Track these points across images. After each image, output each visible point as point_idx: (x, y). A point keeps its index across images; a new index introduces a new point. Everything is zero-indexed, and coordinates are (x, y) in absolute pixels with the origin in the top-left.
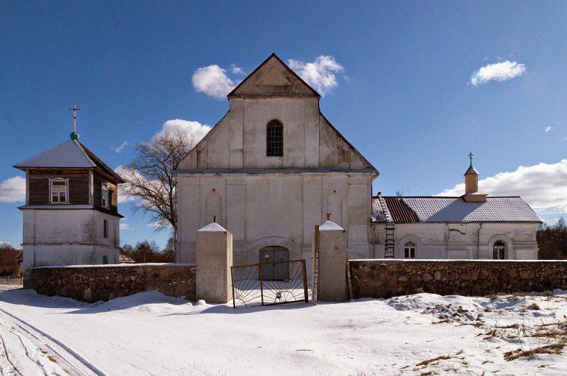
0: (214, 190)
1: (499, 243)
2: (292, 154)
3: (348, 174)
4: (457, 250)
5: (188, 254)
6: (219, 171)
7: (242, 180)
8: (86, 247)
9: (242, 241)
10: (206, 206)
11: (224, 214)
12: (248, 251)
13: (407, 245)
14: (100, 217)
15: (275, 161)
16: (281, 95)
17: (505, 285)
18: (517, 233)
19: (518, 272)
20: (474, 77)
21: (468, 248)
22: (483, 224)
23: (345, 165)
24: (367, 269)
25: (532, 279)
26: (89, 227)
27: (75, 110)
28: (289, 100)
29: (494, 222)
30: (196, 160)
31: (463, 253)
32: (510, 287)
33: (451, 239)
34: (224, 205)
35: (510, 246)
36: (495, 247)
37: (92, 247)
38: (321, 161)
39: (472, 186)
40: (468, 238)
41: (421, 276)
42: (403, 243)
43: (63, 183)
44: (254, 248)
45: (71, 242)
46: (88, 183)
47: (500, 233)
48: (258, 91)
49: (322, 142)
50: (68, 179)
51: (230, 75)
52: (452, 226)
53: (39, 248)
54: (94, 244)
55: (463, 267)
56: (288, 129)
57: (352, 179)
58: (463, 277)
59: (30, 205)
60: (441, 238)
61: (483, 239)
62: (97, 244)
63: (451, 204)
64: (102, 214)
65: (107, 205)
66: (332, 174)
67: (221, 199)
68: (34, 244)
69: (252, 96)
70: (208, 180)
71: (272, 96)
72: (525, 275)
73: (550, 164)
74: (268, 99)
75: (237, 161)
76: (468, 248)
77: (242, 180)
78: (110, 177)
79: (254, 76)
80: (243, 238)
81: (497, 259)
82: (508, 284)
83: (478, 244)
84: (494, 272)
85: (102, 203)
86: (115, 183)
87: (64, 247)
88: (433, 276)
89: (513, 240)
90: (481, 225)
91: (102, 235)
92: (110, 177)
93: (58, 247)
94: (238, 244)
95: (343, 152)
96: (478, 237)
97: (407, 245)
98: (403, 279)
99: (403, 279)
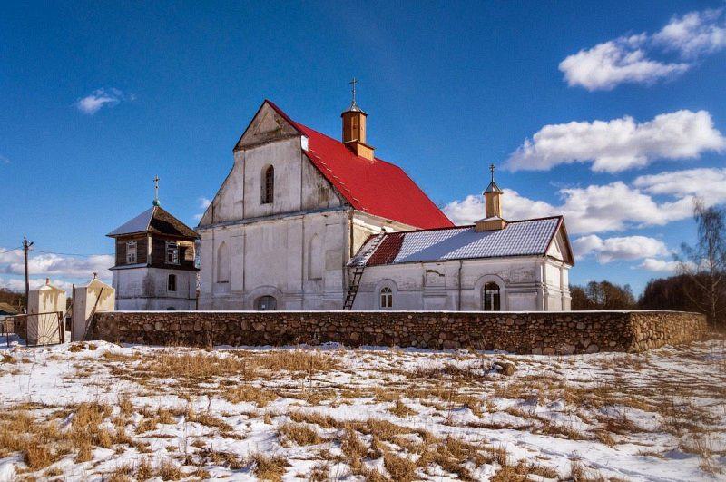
1: (492, 286)
2: (280, 199)
3: (325, 213)
4: (432, 296)
8: (142, 300)
13: (383, 291)
14: (161, 276)
15: (268, 208)
16: (272, 140)
17: (232, 337)
18: (512, 271)
19: (250, 324)
20: (709, 44)
21: (449, 293)
22: (465, 262)
23: (324, 204)
24: (410, 317)
25: (269, 332)
28: (278, 144)
29: (478, 258)
31: (441, 301)
32: (239, 339)
33: (428, 282)
34: (216, 260)
35: (503, 290)
36: (488, 292)
38: (304, 204)
39: (491, 210)
40: (450, 281)
41: (141, 326)
42: (378, 289)
44: (250, 298)
46: (147, 244)
47: (490, 272)
48: (255, 140)
49: (305, 182)
52: (428, 266)
55: (185, 319)
56: (277, 174)
57: (329, 219)
58: (183, 328)
60: (419, 282)
61: (467, 281)
63: (453, 237)
64: (166, 270)
65: (175, 261)
66: (311, 215)
69: (250, 146)
71: (264, 142)
72: (259, 327)
73: (402, 171)
74: (263, 147)
75: (237, 212)
76: (449, 293)
79: (252, 126)
80: (241, 288)
81: (490, 310)
82: (236, 336)
83: (460, 288)
84: (219, 324)
85: (167, 257)
88: (154, 326)
89: (508, 281)
90: (461, 263)
95: (323, 190)
96: (460, 279)
97: (383, 291)
98: (123, 328)
99: (123, 328)
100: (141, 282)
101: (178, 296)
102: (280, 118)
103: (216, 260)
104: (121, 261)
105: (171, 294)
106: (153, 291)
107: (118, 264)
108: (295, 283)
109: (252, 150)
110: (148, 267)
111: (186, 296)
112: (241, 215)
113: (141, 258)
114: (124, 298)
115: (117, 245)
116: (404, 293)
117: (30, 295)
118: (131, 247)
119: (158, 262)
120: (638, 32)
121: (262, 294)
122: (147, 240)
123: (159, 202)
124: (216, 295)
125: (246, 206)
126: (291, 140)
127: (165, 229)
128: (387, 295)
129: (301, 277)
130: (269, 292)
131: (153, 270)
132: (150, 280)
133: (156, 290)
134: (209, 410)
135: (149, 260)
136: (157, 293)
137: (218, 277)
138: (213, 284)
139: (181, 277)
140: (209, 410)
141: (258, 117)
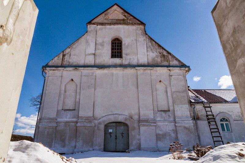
2: (128, 57)
3: (169, 68)
13: (221, 120)
15: (117, 61)
34: (78, 91)
44: (100, 123)
79: (103, 15)
80: (92, 115)
102: (126, 14)
103: (63, 92)
108: (147, 113)
109: (104, 27)
116: (239, 122)
120: (198, 76)
121: (112, 119)
125: (97, 58)
126: (137, 26)
128: (224, 123)
130: (121, 119)
134: (116, 149)
138: (58, 111)
140: (116, 149)
141: (109, 11)
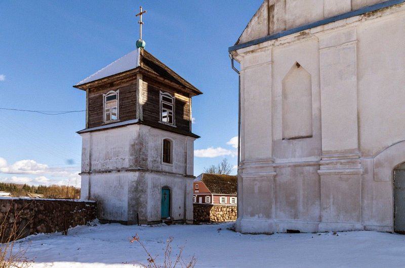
0: (298, 65)
5: (255, 180)
6: (303, 29)
7: (349, 34)
9: (352, 151)
10: (285, 95)
11: (315, 106)
12: (366, 172)
14: (155, 139)
26: (138, 148)
27: (141, 23)
30: (266, 22)
34: (315, 89)
37: (137, 174)
43: (114, 97)
44: (378, 165)
45: (120, 168)
50: (118, 91)
51: (324, 151)
53: (96, 177)
54: (139, 170)
59: (89, 128)
62: (148, 170)
67: (310, 76)
68: (89, 173)
70: (287, 49)
77: (349, 34)
78: (177, 86)
80: (356, 146)
86: (187, 95)
87: (113, 176)
91: (160, 159)
92: (177, 86)
93: (108, 175)
94: (344, 158)
100: (127, 148)
101: (174, 171)
103: (279, 99)
104: (96, 121)
105: (165, 167)
106: (145, 160)
107: (89, 125)
110: (139, 123)
111: (181, 171)
112: (266, 32)
113: (127, 113)
114: (100, 172)
115: (89, 99)
117: (188, 138)
118: (109, 99)
119: (150, 119)
122: (136, 85)
123: (144, 44)
124: (279, 161)
127: (158, 75)
129: (394, 142)
131: (146, 129)
132: (141, 144)
133: (150, 159)
135: (139, 113)
136: (150, 164)
137: (285, 127)
139: (177, 140)
